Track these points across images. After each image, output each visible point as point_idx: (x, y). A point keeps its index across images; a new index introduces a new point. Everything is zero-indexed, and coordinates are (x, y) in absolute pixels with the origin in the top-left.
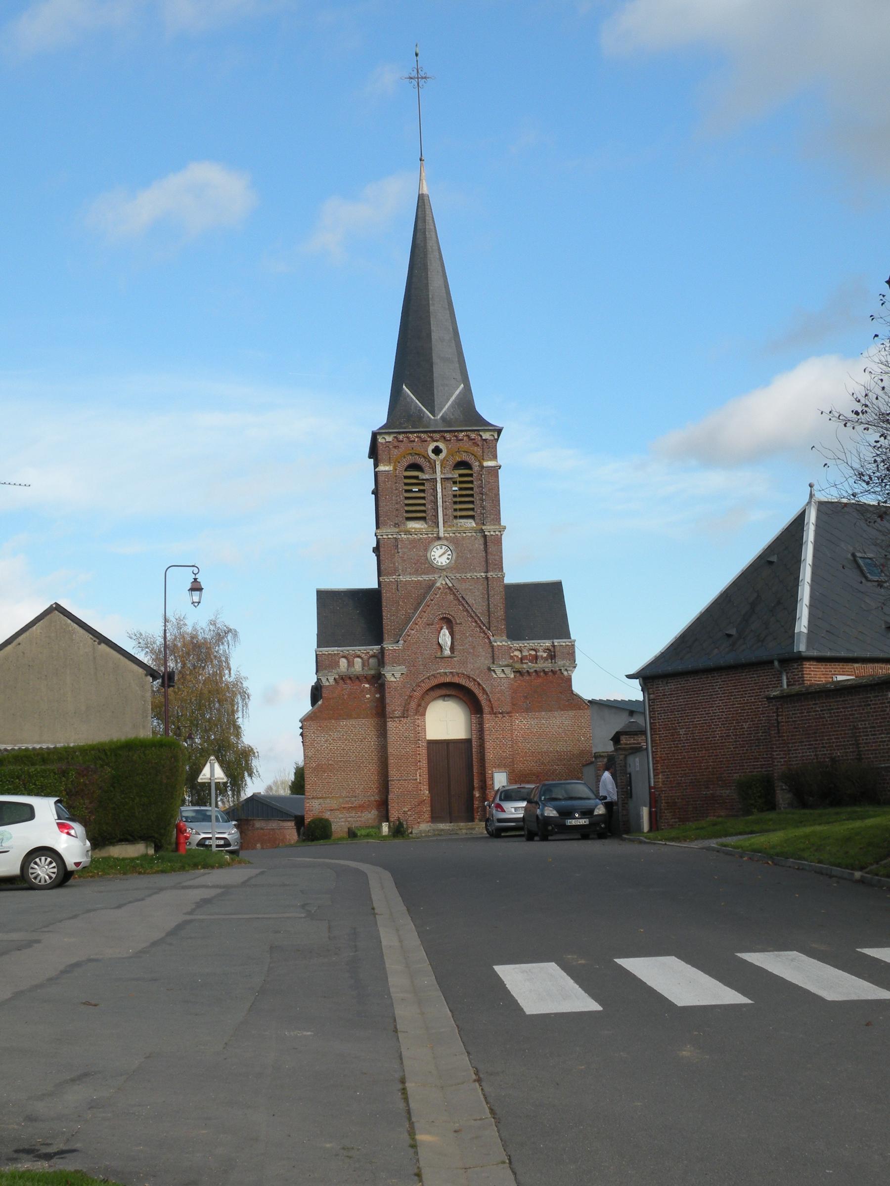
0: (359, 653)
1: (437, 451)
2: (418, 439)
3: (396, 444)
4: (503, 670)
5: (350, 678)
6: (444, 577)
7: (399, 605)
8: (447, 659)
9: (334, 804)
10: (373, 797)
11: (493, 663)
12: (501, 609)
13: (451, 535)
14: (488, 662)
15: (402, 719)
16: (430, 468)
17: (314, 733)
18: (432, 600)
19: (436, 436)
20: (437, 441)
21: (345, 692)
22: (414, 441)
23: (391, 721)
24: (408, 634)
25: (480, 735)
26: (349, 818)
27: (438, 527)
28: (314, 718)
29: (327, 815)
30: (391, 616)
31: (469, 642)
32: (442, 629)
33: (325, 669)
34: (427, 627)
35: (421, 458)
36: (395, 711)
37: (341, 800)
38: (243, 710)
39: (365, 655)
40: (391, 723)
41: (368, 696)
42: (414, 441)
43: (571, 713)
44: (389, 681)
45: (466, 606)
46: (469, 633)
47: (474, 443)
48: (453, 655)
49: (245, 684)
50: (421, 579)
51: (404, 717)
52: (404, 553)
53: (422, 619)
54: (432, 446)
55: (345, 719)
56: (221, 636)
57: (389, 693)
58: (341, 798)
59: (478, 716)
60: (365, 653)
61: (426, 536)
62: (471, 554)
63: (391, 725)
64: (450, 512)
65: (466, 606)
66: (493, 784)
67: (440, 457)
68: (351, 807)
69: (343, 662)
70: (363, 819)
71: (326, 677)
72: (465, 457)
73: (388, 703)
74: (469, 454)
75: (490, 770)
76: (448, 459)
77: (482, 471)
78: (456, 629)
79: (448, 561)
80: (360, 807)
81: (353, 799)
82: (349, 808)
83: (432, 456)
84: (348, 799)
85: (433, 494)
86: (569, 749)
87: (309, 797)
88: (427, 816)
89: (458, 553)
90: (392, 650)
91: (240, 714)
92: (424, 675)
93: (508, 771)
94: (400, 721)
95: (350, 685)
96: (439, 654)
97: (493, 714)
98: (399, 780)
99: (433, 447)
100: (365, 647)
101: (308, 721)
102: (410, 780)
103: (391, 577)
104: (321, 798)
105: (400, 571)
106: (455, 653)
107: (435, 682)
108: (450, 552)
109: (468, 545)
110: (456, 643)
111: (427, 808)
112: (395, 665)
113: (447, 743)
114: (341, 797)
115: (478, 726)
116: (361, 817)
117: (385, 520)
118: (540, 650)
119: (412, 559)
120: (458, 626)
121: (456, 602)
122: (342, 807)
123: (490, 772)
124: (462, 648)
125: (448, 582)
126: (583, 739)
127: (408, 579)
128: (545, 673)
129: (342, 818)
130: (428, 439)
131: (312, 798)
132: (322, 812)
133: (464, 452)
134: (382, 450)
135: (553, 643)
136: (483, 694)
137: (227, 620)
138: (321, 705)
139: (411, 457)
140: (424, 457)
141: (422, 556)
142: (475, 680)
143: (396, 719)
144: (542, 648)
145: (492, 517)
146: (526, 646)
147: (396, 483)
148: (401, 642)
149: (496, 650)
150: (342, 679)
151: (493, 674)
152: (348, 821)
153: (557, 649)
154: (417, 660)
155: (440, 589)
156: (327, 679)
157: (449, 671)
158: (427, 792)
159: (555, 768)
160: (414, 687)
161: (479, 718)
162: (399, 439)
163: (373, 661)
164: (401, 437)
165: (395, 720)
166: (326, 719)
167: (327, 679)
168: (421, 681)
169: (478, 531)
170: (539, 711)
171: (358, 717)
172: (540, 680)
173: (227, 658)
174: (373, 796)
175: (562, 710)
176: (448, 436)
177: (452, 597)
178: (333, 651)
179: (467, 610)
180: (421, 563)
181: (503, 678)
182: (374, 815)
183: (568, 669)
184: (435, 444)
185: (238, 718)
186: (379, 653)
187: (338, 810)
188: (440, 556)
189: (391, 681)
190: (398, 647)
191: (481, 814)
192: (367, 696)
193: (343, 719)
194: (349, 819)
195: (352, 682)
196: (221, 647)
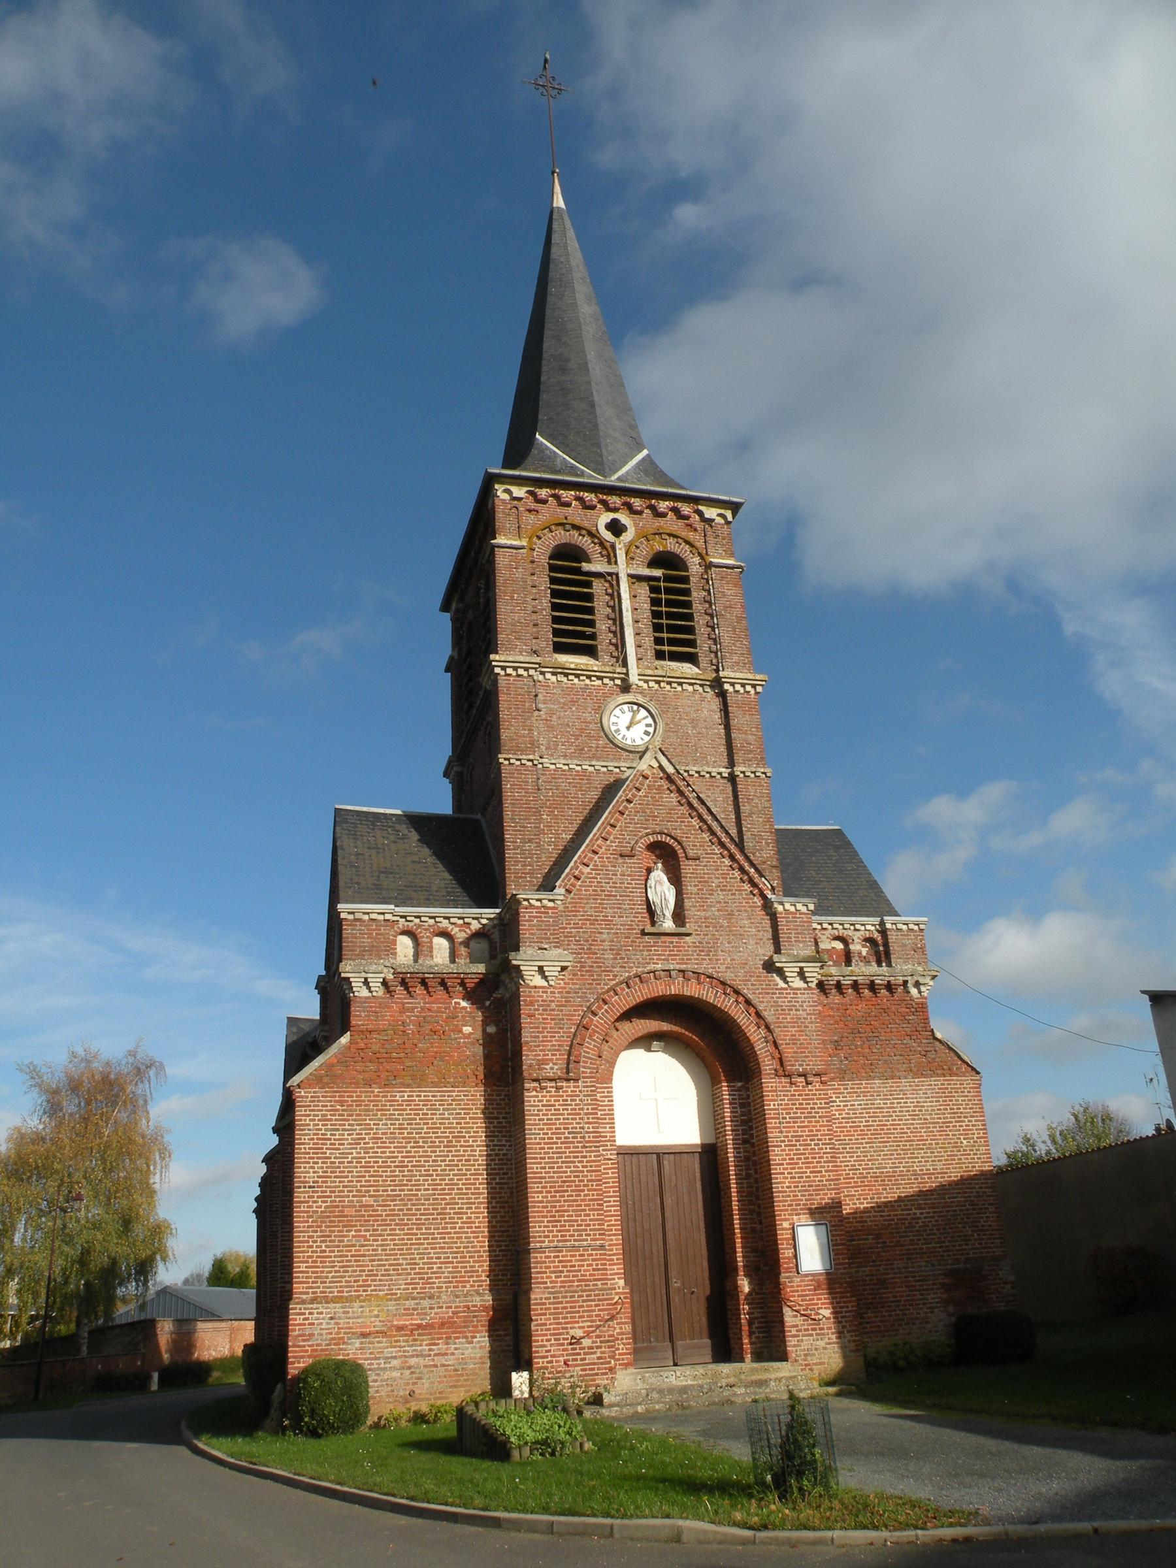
0: (445, 923)
1: (616, 528)
2: (577, 503)
3: (533, 505)
4: (801, 968)
5: (423, 982)
6: (656, 753)
7: (540, 821)
8: (668, 939)
9: (370, 1315)
10: (478, 1298)
11: (778, 950)
12: (768, 844)
13: (652, 684)
14: (767, 950)
15: (564, 1084)
16: (602, 556)
17: (324, 1119)
18: (629, 801)
19: (614, 500)
20: (615, 510)
21: (409, 1017)
22: (568, 505)
23: (535, 1089)
24: (577, 873)
25: (744, 1132)
26: (413, 1356)
27: (625, 664)
28: (325, 1080)
29: (352, 1350)
30: (524, 841)
31: (720, 902)
32: (649, 871)
33: (361, 956)
34: (620, 861)
35: (584, 536)
36: (545, 1062)
37: (391, 1306)
38: (161, 1172)
39: (460, 931)
40: (534, 1093)
41: (467, 1030)
42: (568, 505)
43: (937, 1082)
44: (528, 986)
45: (709, 818)
46: (716, 881)
47: (687, 525)
48: (683, 930)
49: (167, 1138)
50: (591, 769)
51: (568, 1080)
52: (551, 713)
53: (608, 842)
54: (606, 518)
55: (408, 1086)
56: (142, 1069)
57: (530, 1016)
58: (391, 1300)
59: (739, 1084)
60: (461, 926)
61: (599, 682)
62: (694, 727)
63: (535, 1100)
64: (648, 642)
65: (709, 818)
66: (796, 1256)
67: (621, 538)
68: (419, 1326)
69: (405, 945)
70: (451, 1360)
71: (364, 975)
72: (671, 545)
73: (527, 1043)
74: (680, 541)
75: (786, 1220)
76: (637, 544)
77: (706, 572)
78: (687, 868)
79: (647, 738)
80: (442, 1325)
81: (426, 1303)
82: (412, 1331)
83: (608, 536)
84: (411, 1303)
85: (611, 603)
86: (939, 1166)
87: (304, 1297)
88: (623, 1347)
89: (667, 724)
90: (538, 907)
91: (157, 1178)
92: (616, 976)
93: (830, 1222)
94: (558, 1089)
95: (424, 999)
96: (649, 929)
97: (785, 1076)
98: (557, 1249)
99: (609, 521)
100: (460, 910)
101: (310, 1086)
102: (585, 1248)
103: (524, 757)
104: (335, 1300)
105: (543, 748)
106: (688, 925)
107: (641, 993)
108: (650, 721)
109: (688, 709)
110: (687, 904)
111: (622, 1327)
112: (546, 946)
113: (659, 1155)
114: (391, 1296)
115: (739, 1110)
116: (446, 1354)
117: (509, 641)
118: (856, 940)
119: (568, 725)
120: (690, 862)
121: (684, 810)
122: (394, 1326)
123: (786, 1225)
124: (703, 914)
125: (665, 763)
126: (965, 1142)
127: (561, 766)
128: (872, 986)
129: (395, 1358)
130: (599, 506)
131: (313, 1301)
132: (340, 1341)
133: (670, 535)
134: (504, 513)
135: (882, 923)
136: (759, 1027)
137: (151, 1050)
138: (348, 1048)
139: (562, 532)
140: (590, 534)
141: (590, 723)
142: (737, 992)
143: (549, 1084)
144: (858, 934)
145: (735, 658)
146: (825, 929)
147: (533, 574)
148: (560, 891)
149: (782, 922)
150: (404, 983)
151: (778, 979)
152: (409, 1368)
153: (892, 937)
154: (599, 937)
155: (646, 777)
156: (366, 979)
157: (678, 967)
158: (622, 1282)
159: (915, 1214)
160: (593, 1004)
161: (739, 1090)
162: (539, 497)
163: (479, 946)
164: (543, 493)
165: (546, 1088)
166: (357, 1085)
167: (366, 979)
168: (608, 991)
169: (708, 683)
170: (869, 1078)
171: (442, 1081)
172: (862, 1006)
173: (146, 1101)
174: (479, 1294)
175: (916, 1075)
176: (637, 503)
177: (674, 797)
178: (383, 914)
179: (710, 829)
180: (589, 736)
181: (800, 989)
182: (481, 1348)
183: (922, 980)
184: (612, 515)
185: (154, 1183)
186: (494, 926)
187: (383, 1333)
188: (628, 728)
189: (535, 987)
190: (553, 901)
191: (757, 1338)
192: (464, 1029)
193: (404, 1085)
194: (413, 1361)
195: (429, 992)
196: (140, 1086)
